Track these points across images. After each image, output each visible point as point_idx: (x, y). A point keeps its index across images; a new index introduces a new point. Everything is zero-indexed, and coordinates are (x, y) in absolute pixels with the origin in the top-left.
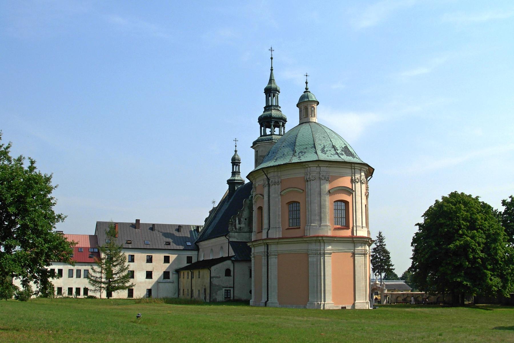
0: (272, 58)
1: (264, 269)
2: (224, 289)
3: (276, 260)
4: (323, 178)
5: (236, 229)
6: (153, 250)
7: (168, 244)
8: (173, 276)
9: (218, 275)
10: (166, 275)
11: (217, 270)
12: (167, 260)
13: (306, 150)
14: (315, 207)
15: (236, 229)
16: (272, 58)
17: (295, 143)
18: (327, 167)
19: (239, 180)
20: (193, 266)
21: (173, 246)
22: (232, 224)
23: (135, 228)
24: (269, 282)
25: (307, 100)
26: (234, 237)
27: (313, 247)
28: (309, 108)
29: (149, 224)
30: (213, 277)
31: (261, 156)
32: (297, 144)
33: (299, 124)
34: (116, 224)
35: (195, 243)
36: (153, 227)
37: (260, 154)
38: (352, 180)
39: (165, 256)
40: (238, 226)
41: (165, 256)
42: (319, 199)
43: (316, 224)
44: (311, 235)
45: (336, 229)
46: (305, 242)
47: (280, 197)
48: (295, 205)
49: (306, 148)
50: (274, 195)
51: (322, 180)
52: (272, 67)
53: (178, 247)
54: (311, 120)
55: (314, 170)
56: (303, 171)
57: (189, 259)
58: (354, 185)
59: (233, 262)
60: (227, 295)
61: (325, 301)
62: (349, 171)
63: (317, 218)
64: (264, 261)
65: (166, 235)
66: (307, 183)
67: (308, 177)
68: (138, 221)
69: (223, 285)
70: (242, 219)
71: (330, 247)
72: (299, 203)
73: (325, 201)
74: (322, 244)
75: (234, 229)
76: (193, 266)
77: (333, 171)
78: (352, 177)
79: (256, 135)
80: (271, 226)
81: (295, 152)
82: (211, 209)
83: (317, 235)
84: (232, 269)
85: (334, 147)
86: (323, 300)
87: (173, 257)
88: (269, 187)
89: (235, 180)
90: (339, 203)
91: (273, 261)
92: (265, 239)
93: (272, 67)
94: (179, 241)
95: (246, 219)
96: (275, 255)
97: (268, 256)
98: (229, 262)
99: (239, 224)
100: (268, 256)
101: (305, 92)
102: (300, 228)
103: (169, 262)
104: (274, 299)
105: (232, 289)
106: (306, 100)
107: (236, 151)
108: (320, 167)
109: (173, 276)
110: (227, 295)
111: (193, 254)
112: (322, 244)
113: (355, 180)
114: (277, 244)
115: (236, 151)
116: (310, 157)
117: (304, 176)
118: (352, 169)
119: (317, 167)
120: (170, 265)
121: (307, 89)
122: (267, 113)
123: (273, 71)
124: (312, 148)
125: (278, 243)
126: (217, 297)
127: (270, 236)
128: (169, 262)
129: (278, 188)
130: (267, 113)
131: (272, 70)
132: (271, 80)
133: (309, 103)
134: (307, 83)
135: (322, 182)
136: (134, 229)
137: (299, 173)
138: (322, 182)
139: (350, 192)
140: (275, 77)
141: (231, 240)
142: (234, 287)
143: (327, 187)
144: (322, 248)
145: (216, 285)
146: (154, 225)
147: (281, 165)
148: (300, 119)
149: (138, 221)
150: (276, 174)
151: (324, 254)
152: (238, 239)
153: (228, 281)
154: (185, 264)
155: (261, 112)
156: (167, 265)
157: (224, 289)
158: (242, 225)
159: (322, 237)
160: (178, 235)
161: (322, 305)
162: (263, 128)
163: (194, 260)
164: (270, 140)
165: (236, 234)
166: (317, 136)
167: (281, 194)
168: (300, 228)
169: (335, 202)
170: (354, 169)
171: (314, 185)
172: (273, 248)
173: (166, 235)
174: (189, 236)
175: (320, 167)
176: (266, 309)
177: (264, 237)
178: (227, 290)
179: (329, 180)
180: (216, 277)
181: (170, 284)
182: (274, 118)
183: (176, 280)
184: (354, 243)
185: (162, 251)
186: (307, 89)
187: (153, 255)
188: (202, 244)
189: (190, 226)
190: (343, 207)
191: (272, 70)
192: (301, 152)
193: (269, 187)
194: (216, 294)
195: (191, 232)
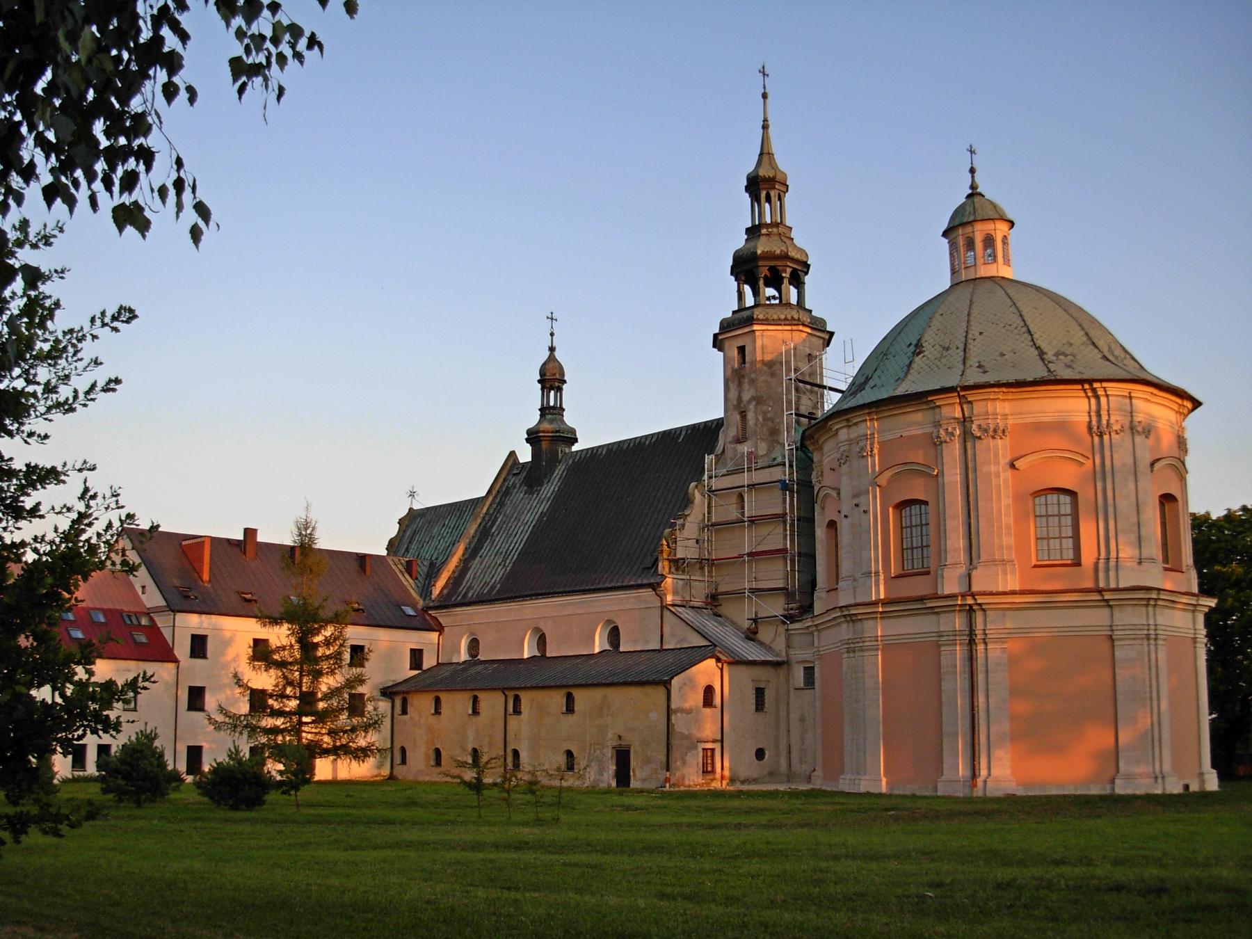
0: (765, 96)
30: (676, 711)
42: (1132, 486)
48: (915, 509)
52: (765, 120)
57: (417, 655)
58: (969, 445)
67: (1104, 422)
68: (250, 533)
82: (404, 512)
90: (1053, 498)
93: (765, 120)
101: (969, 196)
105: (717, 746)
107: (552, 349)
115: (552, 349)
117: (930, 430)
121: (973, 187)
123: (770, 130)
131: (765, 127)
132: (765, 154)
142: (722, 741)
148: (954, 272)
149: (250, 533)
163: (429, 662)
184: (1110, 606)
186: (973, 187)
190: (1067, 509)
191: (765, 127)
194: (684, 763)
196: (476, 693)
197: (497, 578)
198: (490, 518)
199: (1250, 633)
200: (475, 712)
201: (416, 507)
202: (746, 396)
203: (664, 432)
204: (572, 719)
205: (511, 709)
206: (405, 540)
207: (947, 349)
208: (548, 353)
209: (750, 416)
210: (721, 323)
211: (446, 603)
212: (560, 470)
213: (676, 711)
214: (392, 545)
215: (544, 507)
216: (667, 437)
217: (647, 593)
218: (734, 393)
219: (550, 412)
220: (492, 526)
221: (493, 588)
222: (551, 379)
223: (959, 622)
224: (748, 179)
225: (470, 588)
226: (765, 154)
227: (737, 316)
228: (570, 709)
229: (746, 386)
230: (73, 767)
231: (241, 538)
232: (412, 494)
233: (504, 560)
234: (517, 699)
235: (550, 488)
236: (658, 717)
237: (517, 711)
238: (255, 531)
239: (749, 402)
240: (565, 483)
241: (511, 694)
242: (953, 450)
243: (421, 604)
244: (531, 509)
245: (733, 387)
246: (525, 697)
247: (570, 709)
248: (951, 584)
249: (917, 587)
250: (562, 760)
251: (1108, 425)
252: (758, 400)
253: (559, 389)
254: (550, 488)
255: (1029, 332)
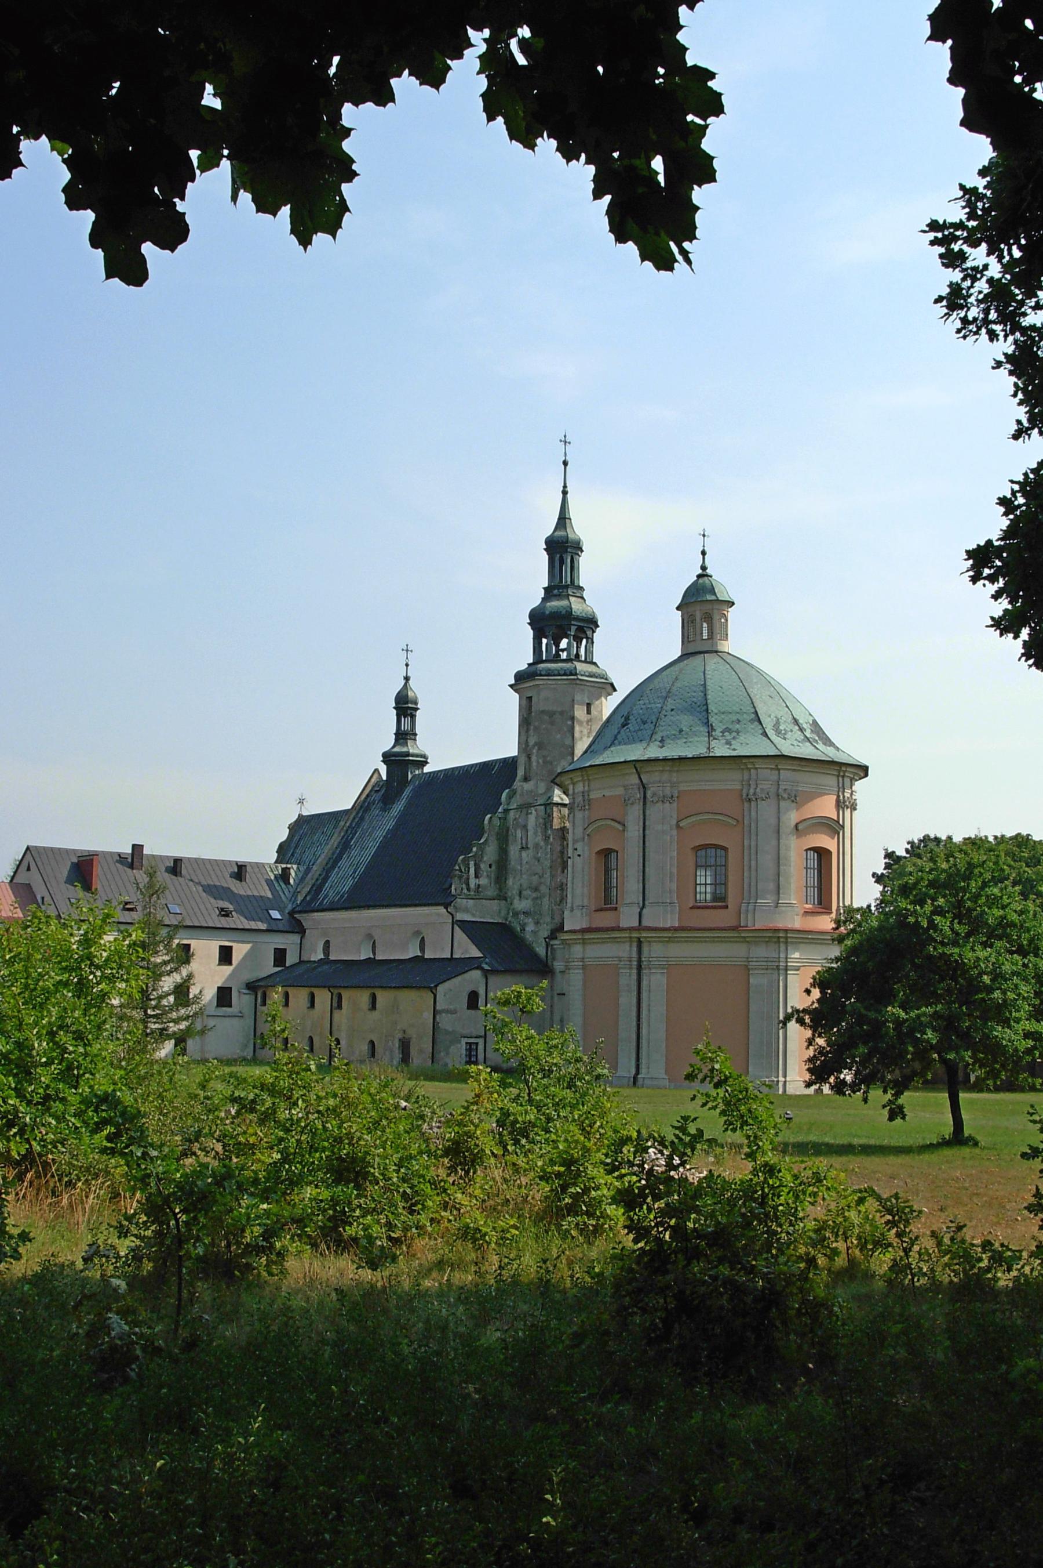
0: (565, 463)
1: (627, 1000)
2: (464, 1041)
3: (580, 977)
4: (786, 796)
5: (468, 889)
6: (198, 931)
7: (225, 913)
8: (241, 1001)
9: (452, 1007)
10: (224, 996)
11: (452, 991)
12: (225, 956)
13: (738, 726)
14: (766, 860)
15: (468, 889)
16: (565, 463)
17: (707, 704)
18: (794, 770)
19: (417, 756)
20: (290, 973)
21: (238, 921)
22: (460, 877)
23: (131, 866)
24: (644, 1031)
25: (713, 598)
26: (466, 910)
27: (761, 952)
28: (716, 617)
29: (67, 851)
30: (440, 1012)
31: (543, 712)
32: (711, 707)
33: (685, 656)
34: (96, 854)
35: (291, 914)
36: (176, 867)
37: (538, 705)
38: (838, 801)
39: (221, 947)
40: (473, 882)
41: (221, 947)
42: (774, 842)
43: (767, 901)
44: (757, 927)
45: (807, 913)
46: (744, 940)
47: (674, 832)
49: (739, 721)
50: (660, 827)
51: (784, 799)
52: (565, 486)
53: (253, 925)
54: (720, 648)
55: (766, 779)
56: (736, 775)
57: (280, 955)
59: (486, 974)
60: (470, 1056)
61: (785, 1076)
62: (832, 781)
63: (772, 886)
64: (627, 978)
65: (214, 891)
66: (746, 804)
67: (752, 791)
68: (137, 848)
69: (465, 1032)
70: (482, 866)
71: (797, 955)
72: (725, 849)
73: (788, 849)
74: (782, 947)
75: (465, 891)
76: (290, 973)
77: (806, 780)
78: (838, 796)
79: (524, 658)
80: (651, 897)
81: (713, 730)
83: (780, 925)
84: (482, 992)
85: (796, 721)
86: (781, 1072)
87: (240, 950)
88: (645, 804)
89: (408, 754)
91: (656, 981)
92: (631, 929)
93: (565, 486)
94: (255, 907)
95: (490, 866)
96: (661, 967)
97: (639, 968)
98: (476, 974)
99: (477, 876)
100: (639, 968)
101: (699, 576)
102: (726, 907)
103: (230, 964)
104: (655, 1068)
105: (481, 1041)
106: (709, 597)
107: (407, 679)
108: (779, 770)
109: (241, 1001)
110: (470, 1056)
111: (289, 942)
112: (782, 947)
113: (844, 802)
114: (667, 942)
115: (407, 679)
116: (750, 745)
118: (838, 776)
119: (772, 769)
120: (233, 971)
121: (704, 568)
122: (555, 604)
124: (752, 721)
125: (670, 940)
126: (448, 1060)
127: (646, 923)
128: (230, 964)
129: (670, 810)
130: (555, 604)
131: (565, 493)
132: (563, 520)
133: (716, 606)
134: (704, 553)
135: (782, 804)
136: (129, 870)
137: (730, 781)
138: (782, 804)
139: (834, 828)
140: (573, 513)
141: (459, 916)
143: (793, 817)
144: (782, 955)
145: (447, 1032)
146: (177, 861)
147: (686, 758)
149: (137, 848)
150: (665, 776)
151: (786, 969)
152: (474, 915)
153: (470, 1023)
154: (269, 968)
155: (536, 597)
156: (228, 970)
157: (464, 1041)
158: (483, 881)
159: (786, 931)
160: (242, 893)
161: (781, 1085)
162: (544, 641)
163: (291, 959)
164: (571, 674)
165: (471, 901)
166: (753, 692)
167: (678, 826)
168: (726, 907)
169: (806, 850)
170: (843, 777)
171: (766, 810)
172: (654, 951)
173: (214, 891)
174: (270, 895)
175: (779, 770)
176: (633, 1091)
177: (628, 918)
178: (470, 1044)
179: (796, 799)
180: (448, 1011)
181: (235, 1022)
182: (578, 619)
183: (248, 1011)
185: (206, 932)
186: (704, 568)
187: (194, 944)
188: (308, 920)
189: (263, 865)
191: (565, 493)
192: (728, 730)
193: (645, 804)
194: (448, 1054)
195: (269, 882)
196: (313, 989)
197: (347, 888)
198: (352, 830)
199: (5, 1158)
200: (312, 1005)
201: (305, 813)
202: (532, 742)
203: (485, 763)
204: (376, 1015)
205: (335, 1005)
206: (293, 845)
207: (644, 723)
208: (403, 682)
209: (534, 758)
210: (516, 676)
211: (308, 907)
212: (407, 792)
213: (440, 1012)
214: (283, 850)
215: (391, 824)
216: (486, 766)
217: (442, 910)
218: (524, 738)
219: (403, 736)
220: (352, 839)
221: (342, 896)
222: (405, 707)
223: (625, 951)
224: (546, 543)
225: (326, 896)
226: (563, 520)
227: (533, 668)
228: (373, 1006)
229: (531, 732)
230: (220, 960)
231: (130, 851)
232: (301, 801)
233: (355, 872)
234: (340, 996)
235: (398, 807)
236: (428, 1016)
237: (340, 1007)
238: (142, 846)
239: (534, 746)
240: (408, 806)
241: (336, 991)
242: (634, 813)
243: (290, 907)
244: (384, 823)
245: (523, 733)
246: (346, 995)
247: (373, 1006)
248: (628, 918)
249: (605, 920)
250: (365, 1047)
251: (754, 794)
252: (540, 745)
253: (413, 717)
254: (398, 807)
255: (707, 710)
